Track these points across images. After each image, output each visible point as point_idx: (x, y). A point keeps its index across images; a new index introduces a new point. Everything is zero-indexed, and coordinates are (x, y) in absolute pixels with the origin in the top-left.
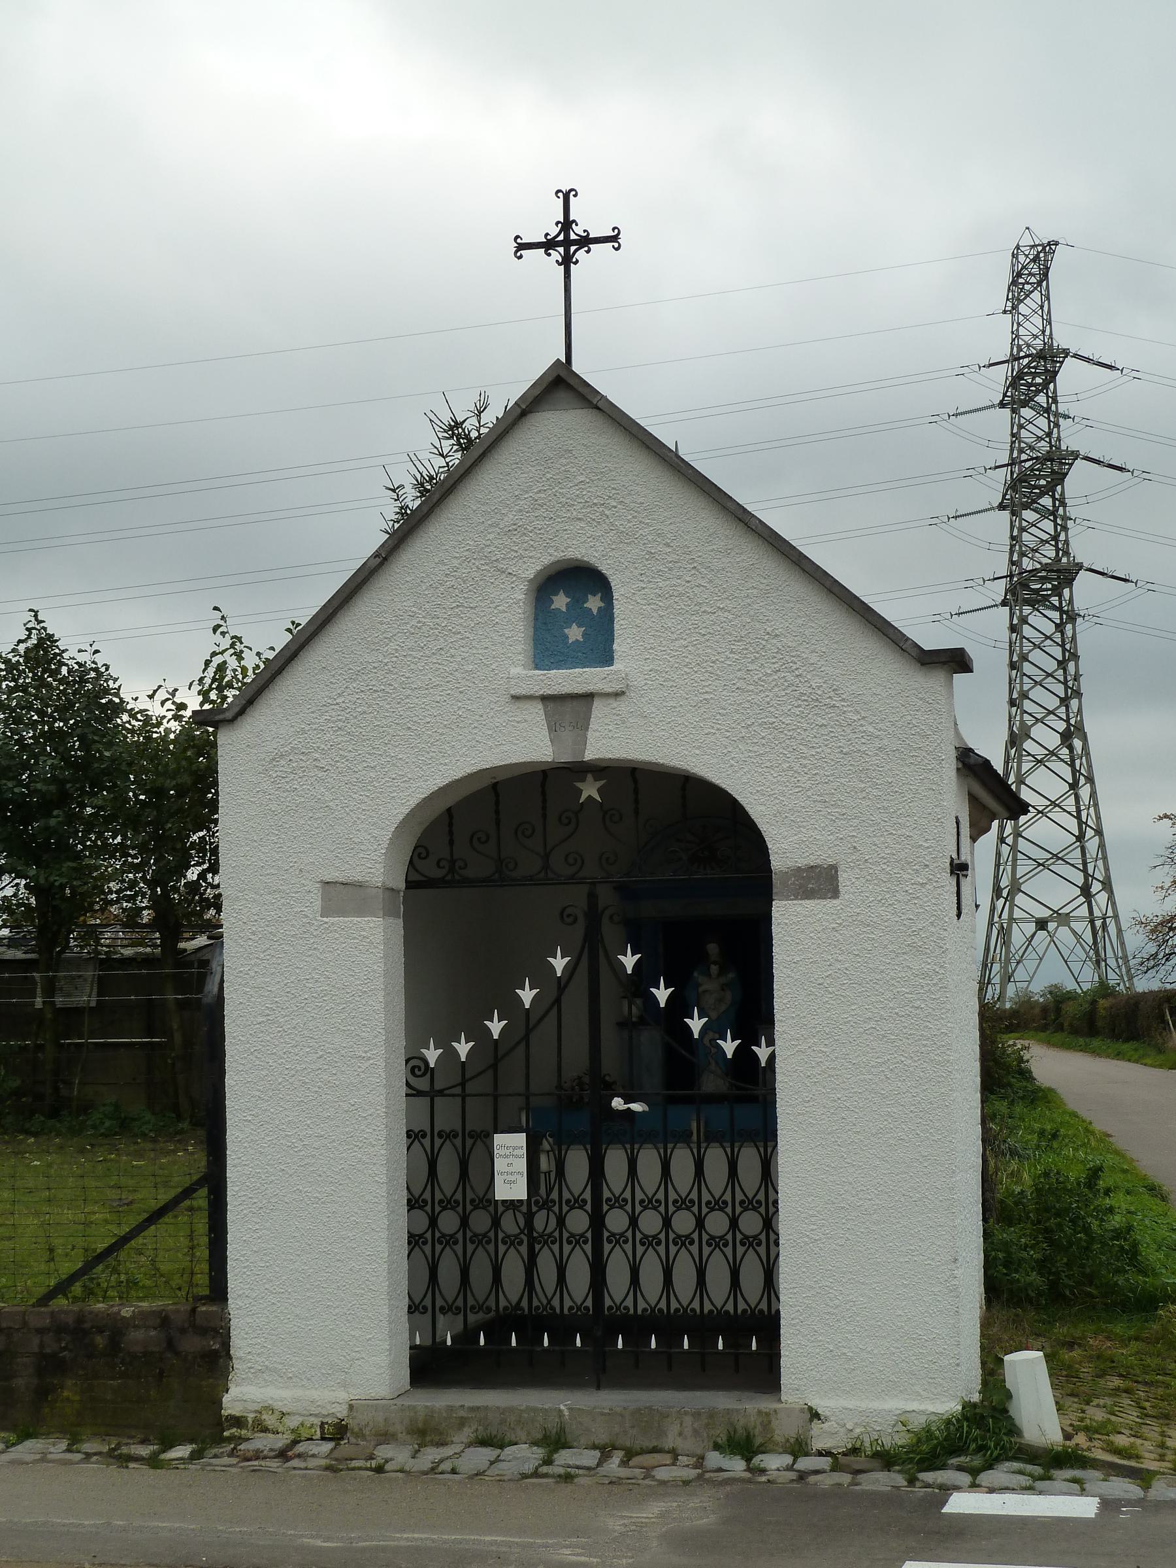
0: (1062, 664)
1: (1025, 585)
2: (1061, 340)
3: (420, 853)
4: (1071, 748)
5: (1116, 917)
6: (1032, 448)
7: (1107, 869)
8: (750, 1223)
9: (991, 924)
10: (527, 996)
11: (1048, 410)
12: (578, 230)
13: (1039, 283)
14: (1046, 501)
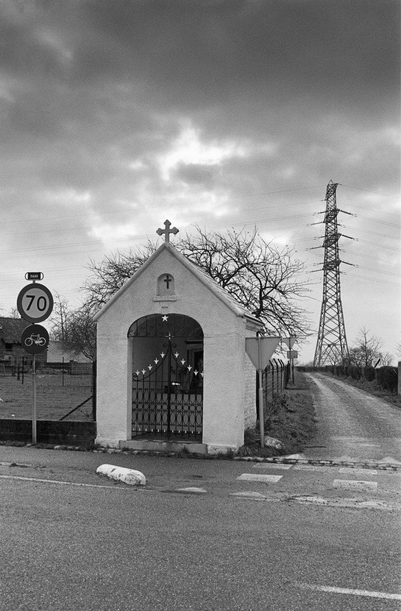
0: (336, 284)
1: (328, 265)
2: (338, 207)
4: (338, 304)
5: (347, 344)
6: (330, 233)
7: (345, 333)
8: (199, 408)
9: (317, 345)
10: (156, 362)
11: (335, 224)
13: (333, 193)
14: (334, 245)
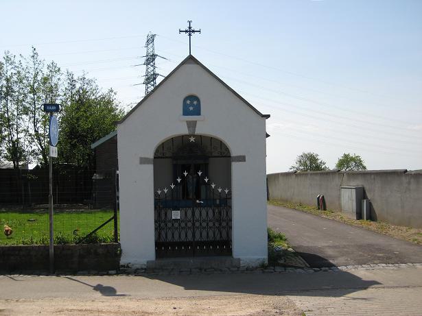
12: (187, 29)
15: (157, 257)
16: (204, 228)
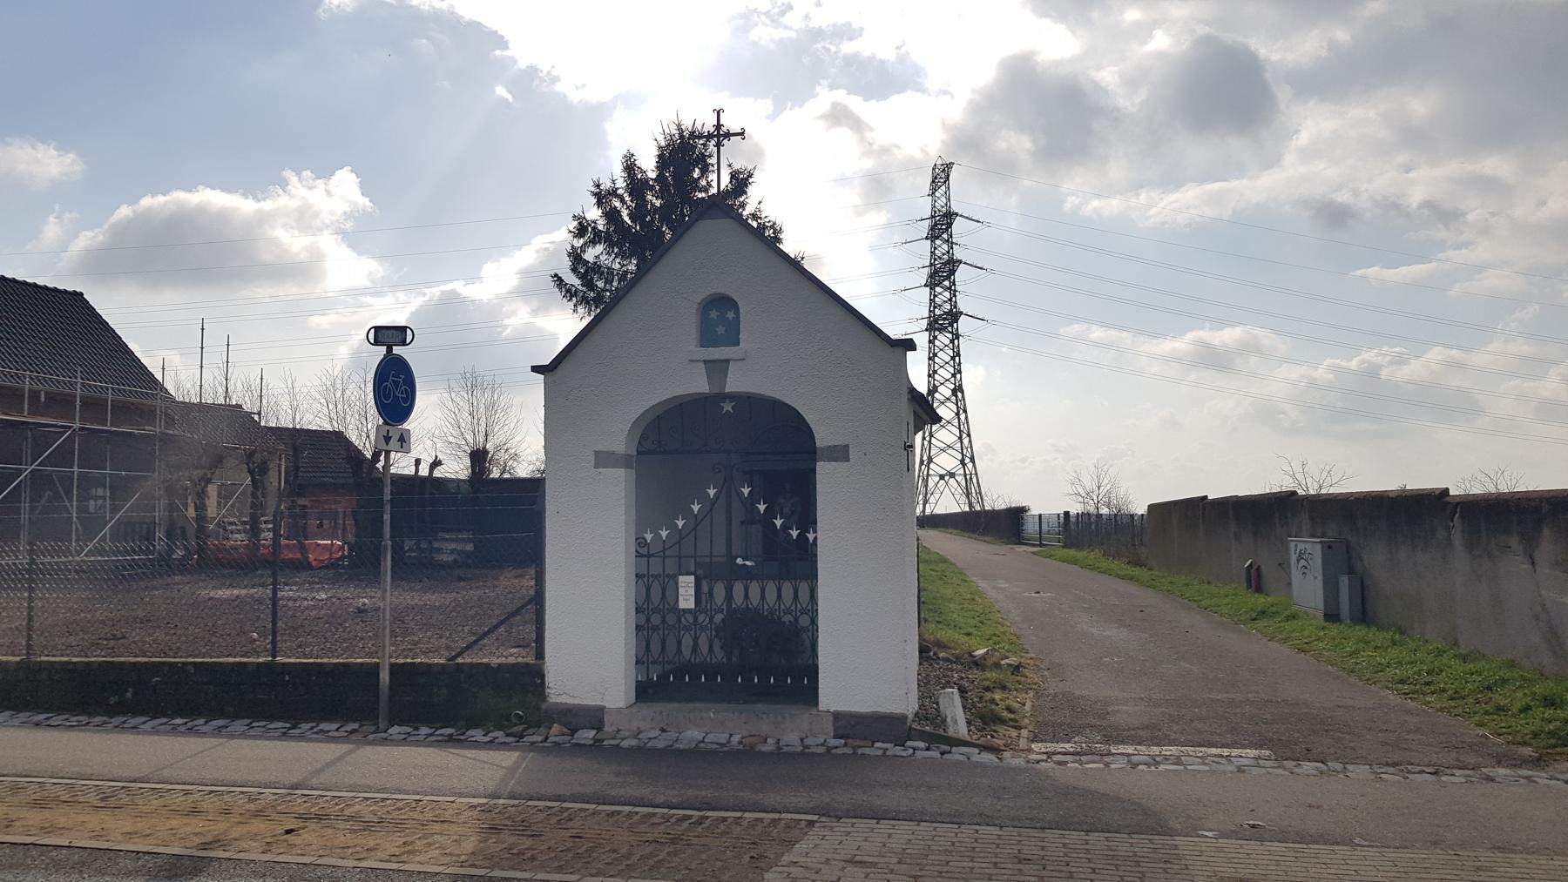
1: (936, 321)
2: (955, 208)
3: (644, 437)
10: (696, 508)
14: (946, 283)
15: (838, 716)
16: (656, 628)
